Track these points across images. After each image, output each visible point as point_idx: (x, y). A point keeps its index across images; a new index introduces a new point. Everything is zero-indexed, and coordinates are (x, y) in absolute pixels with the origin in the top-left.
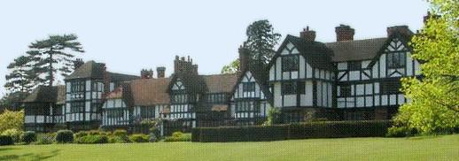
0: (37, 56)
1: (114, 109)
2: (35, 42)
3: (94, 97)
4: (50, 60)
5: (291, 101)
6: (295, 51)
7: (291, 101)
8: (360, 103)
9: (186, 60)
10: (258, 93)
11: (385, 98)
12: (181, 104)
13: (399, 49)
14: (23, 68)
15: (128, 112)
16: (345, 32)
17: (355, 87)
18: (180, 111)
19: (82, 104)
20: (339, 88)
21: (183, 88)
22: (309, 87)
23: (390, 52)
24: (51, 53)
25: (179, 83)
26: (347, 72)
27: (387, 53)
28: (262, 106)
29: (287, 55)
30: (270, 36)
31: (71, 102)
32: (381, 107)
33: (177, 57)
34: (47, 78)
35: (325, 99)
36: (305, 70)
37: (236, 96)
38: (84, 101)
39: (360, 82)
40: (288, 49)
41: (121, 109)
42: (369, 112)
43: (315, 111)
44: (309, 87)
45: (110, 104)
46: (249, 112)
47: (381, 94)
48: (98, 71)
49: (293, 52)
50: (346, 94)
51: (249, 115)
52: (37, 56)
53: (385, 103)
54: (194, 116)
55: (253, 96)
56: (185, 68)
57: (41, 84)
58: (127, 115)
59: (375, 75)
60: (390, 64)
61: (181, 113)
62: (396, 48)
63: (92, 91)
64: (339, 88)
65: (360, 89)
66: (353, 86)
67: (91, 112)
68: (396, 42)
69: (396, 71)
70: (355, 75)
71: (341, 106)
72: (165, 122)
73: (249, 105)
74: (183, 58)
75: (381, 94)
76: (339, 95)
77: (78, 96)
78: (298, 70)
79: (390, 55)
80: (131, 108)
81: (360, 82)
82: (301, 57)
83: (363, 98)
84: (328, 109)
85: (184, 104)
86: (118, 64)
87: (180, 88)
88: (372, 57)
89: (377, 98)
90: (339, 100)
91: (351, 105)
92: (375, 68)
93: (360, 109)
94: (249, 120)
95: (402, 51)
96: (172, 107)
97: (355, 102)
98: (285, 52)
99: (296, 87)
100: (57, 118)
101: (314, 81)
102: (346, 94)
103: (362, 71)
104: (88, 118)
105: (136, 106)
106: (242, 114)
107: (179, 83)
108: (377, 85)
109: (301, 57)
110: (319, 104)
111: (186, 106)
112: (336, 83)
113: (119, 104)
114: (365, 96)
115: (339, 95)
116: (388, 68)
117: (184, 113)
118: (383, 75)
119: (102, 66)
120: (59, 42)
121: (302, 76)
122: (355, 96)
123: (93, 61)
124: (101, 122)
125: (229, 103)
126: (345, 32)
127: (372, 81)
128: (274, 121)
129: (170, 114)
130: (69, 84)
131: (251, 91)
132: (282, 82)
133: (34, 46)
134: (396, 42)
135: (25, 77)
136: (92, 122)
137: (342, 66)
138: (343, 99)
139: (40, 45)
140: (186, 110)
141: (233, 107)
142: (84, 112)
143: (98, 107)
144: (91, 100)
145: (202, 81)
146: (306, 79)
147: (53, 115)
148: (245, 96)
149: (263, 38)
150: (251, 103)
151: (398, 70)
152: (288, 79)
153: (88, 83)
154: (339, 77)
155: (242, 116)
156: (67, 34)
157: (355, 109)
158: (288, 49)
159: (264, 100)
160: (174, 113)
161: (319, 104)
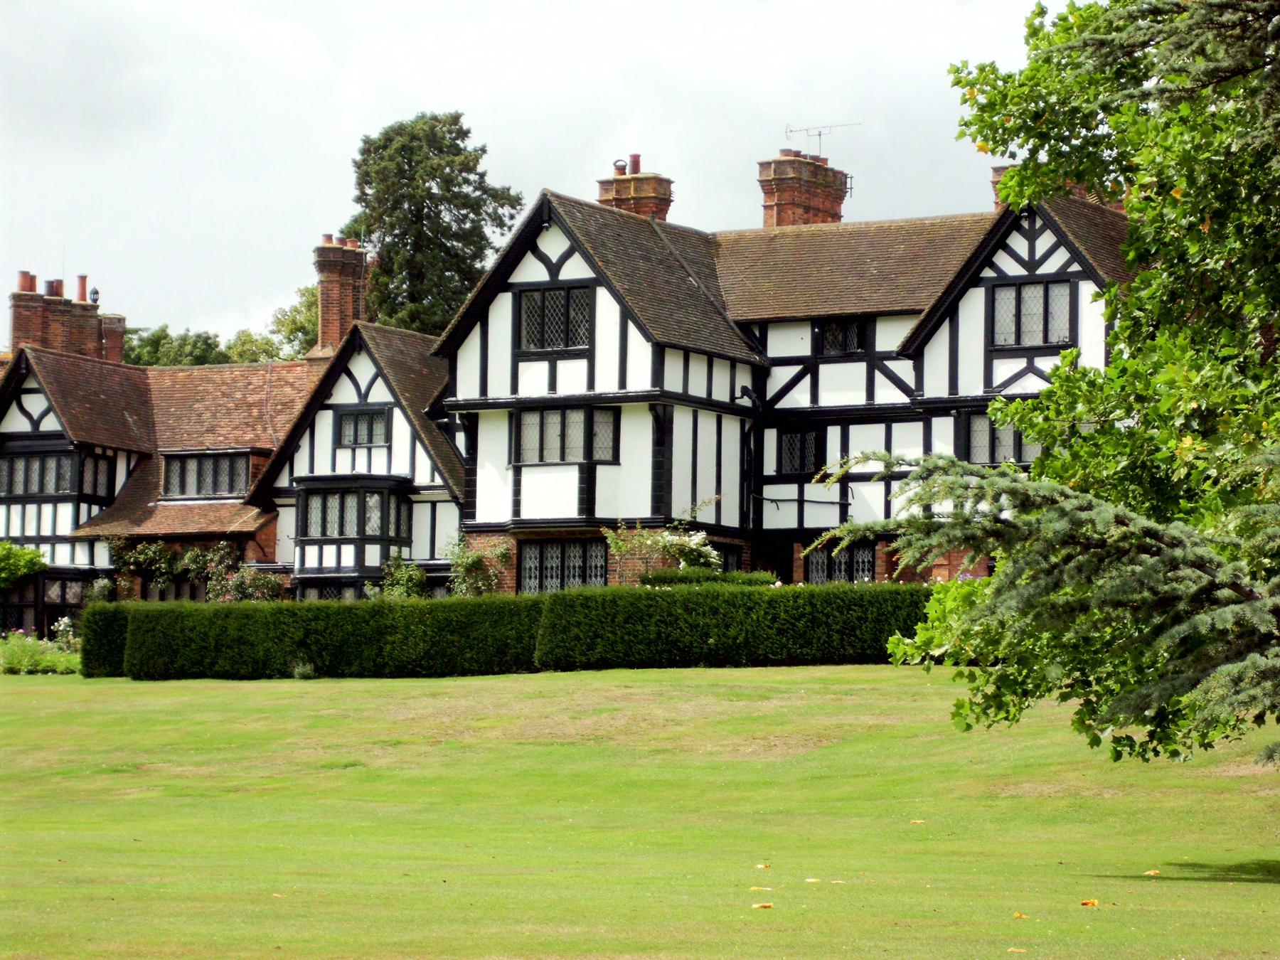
12: (40, 499)
16: (805, 186)
20: (771, 436)
21: (51, 424)
22: (637, 434)
23: (1004, 281)
26: (809, 367)
27: (992, 290)
28: (421, 514)
37: (301, 469)
39: (871, 414)
44: (637, 434)
46: (361, 542)
51: (360, 556)
54: (103, 560)
55: (379, 469)
64: (771, 436)
65: (866, 437)
66: (834, 433)
68: (1032, 237)
69: (1031, 369)
70: (842, 385)
71: (779, 517)
74: (55, 287)
76: (770, 468)
81: (871, 414)
85: (56, 500)
90: (770, 491)
92: (937, 352)
95: (1061, 277)
98: (531, 271)
101: (661, 406)
103: (876, 362)
106: (330, 550)
108: (944, 428)
109: (604, 298)
111: (66, 510)
112: (759, 414)
115: (770, 468)
116: (993, 351)
117: (55, 540)
121: (607, 384)
127: (922, 411)
134: (1032, 237)
137: (791, 343)
138: (791, 490)
140: (65, 528)
141: (287, 519)
148: (344, 469)
154: (773, 388)
155: (330, 561)
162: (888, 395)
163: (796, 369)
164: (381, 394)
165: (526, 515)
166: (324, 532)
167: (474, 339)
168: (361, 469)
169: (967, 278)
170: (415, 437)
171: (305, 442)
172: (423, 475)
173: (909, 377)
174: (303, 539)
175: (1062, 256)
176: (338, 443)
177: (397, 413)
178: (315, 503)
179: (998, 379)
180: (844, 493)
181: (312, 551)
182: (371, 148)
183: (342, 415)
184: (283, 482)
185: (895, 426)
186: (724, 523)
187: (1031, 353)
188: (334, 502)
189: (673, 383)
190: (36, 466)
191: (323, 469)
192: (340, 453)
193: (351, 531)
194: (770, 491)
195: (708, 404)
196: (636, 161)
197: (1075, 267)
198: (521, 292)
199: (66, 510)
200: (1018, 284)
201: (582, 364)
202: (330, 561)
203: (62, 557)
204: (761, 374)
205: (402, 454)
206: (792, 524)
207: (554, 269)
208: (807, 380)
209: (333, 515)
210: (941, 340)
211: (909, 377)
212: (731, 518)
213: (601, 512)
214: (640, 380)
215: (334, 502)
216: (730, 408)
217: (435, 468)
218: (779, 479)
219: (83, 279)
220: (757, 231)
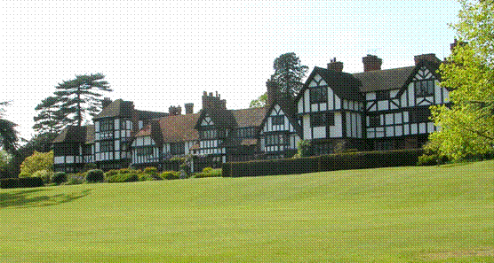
0: (65, 96)
2: (61, 83)
3: (123, 135)
4: (78, 100)
5: (320, 132)
6: (323, 83)
7: (320, 132)
8: (390, 133)
9: (214, 95)
10: (287, 126)
12: (210, 140)
16: (372, 62)
18: (209, 147)
19: (111, 143)
20: (368, 118)
21: (211, 123)
22: (338, 119)
24: (78, 93)
25: (208, 119)
26: (376, 102)
28: (292, 139)
31: (101, 141)
32: (410, 136)
34: (76, 118)
35: (355, 131)
36: (333, 101)
37: (265, 130)
38: (113, 140)
39: (389, 111)
44: (338, 119)
45: (139, 142)
46: (279, 145)
47: (410, 123)
50: (375, 124)
52: (65, 96)
53: (414, 131)
54: (224, 152)
55: (282, 129)
58: (156, 151)
59: (404, 105)
60: (419, 92)
63: (121, 129)
64: (368, 118)
65: (389, 119)
66: (382, 116)
67: (121, 151)
68: (424, 71)
69: (425, 100)
70: (383, 105)
72: (195, 158)
73: (279, 139)
74: (211, 94)
75: (410, 123)
77: (103, 136)
78: (326, 101)
79: (418, 83)
80: (160, 145)
81: (389, 111)
84: (357, 139)
89: (406, 126)
90: (368, 130)
91: (380, 135)
92: (404, 97)
93: (390, 139)
94: (278, 153)
96: (201, 143)
99: (325, 119)
100: (87, 158)
101: (343, 112)
103: (390, 100)
104: (117, 157)
107: (208, 119)
108: (406, 114)
109: (329, 88)
111: (216, 142)
112: (365, 113)
113: (148, 142)
114: (394, 125)
116: (416, 96)
118: (412, 104)
119: (130, 104)
121: (331, 108)
122: (384, 126)
125: (258, 137)
126: (372, 62)
127: (401, 110)
128: (304, 154)
129: (199, 150)
132: (311, 114)
133: (62, 86)
134: (424, 71)
135: (53, 117)
137: (371, 97)
139: (67, 85)
140: (216, 145)
141: (263, 141)
142: (114, 151)
143: (128, 145)
144: (120, 138)
147: (83, 156)
148: (274, 130)
149: (291, 70)
151: (427, 98)
153: (117, 122)
157: (385, 139)
159: (293, 133)
160: (204, 149)
161: (349, 135)
162: (393, 107)
164: (282, 113)
169: (410, 80)
184: (262, 133)
191: (270, 130)
198: (311, 89)
199: (216, 142)
204: (365, 103)
210: (404, 95)
214: (338, 107)
216: (358, 112)
218: (371, 127)
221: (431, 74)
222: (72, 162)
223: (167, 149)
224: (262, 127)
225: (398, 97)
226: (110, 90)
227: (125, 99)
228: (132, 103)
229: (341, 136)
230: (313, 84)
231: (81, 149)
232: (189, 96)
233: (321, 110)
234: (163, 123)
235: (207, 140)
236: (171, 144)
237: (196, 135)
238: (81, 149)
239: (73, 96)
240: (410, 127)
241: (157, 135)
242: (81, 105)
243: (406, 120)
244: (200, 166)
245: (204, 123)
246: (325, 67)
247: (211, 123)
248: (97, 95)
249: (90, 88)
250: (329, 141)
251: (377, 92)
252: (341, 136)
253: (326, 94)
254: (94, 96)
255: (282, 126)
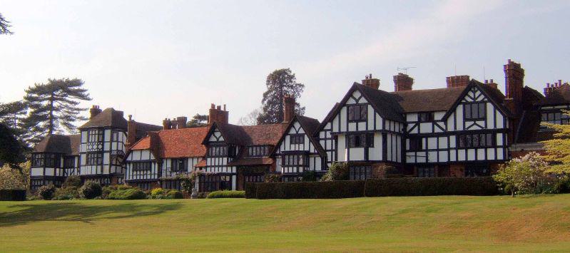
0: (36, 103)
1: (139, 162)
2: (33, 86)
3: (114, 148)
4: (50, 108)
5: (358, 154)
6: (363, 101)
7: (358, 154)
8: (433, 158)
9: (222, 109)
10: (307, 145)
11: (462, 153)
12: (219, 157)
13: (479, 99)
14: (17, 116)
15: (157, 165)
16: (403, 81)
17: (427, 141)
18: (219, 165)
19: (100, 156)
20: (408, 141)
21: (222, 139)
22: (378, 140)
23: (468, 103)
24: (52, 99)
25: (218, 134)
26: (418, 124)
27: (464, 104)
28: (312, 160)
29: (353, 105)
30: (292, 87)
31: (88, 153)
32: (457, 163)
33: (213, 106)
34: (46, 127)
35: (394, 155)
36: (374, 121)
37: (282, 149)
38: (102, 152)
39: (433, 135)
40: (355, 99)
41: (149, 162)
42: (443, 167)
43: (496, 177)
44: (378, 140)
45: (136, 156)
46: (298, 166)
47: (457, 148)
48: (116, 121)
49: (360, 102)
50: (417, 146)
51: (298, 170)
52: (36, 103)
53: (462, 158)
54: (234, 171)
55: (301, 149)
56: (218, 115)
57: (38, 134)
58: (155, 168)
59: (451, 128)
60: (468, 116)
61: (219, 166)
62: (474, 99)
63: (112, 141)
64: (408, 141)
65: (432, 143)
66: (424, 140)
67: (111, 165)
68: (474, 92)
69: (475, 124)
70: (426, 128)
71: (410, 160)
72: (201, 176)
73: (298, 160)
74: (219, 107)
75: (457, 148)
76: (408, 148)
77: (90, 147)
78: (366, 120)
79: (468, 107)
80: (160, 161)
81: (433, 135)
82: (370, 107)
83: (440, 152)
84: (396, 163)
85: (223, 157)
86: (148, 113)
87: (218, 139)
88: (447, 107)
89: (453, 153)
90: (407, 154)
91: (421, 160)
92: (336, 122)
93: (433, 164)
94: (298, 174)
95: (482, 101)
96: (209, 159)
97: (427, 157)
98: (351, 101)
99: (359, 140)
100: (69, 171)
101: (384, 133)
102: (417, 146)
103: (435, 123)
104: (106, 172)
105: (167, 159)
106: (291, 168)
107: (218, 134)
108: (453, 138)
109: (370, 107)
110: (389, 159)
111: (225, 159)
112: (405, 135)
113: (146, 156)
114: (438, 150)
115: (408, 148)
116: (465, 119)
117: (222, 166)
118: (460, 128)
119: (120, 114)
120: (68, 88)
121: (371, 128)
122: (427, 151)
123: (113, 109)
124: (122, 176)
125: (273, 156)
126: (403, 81)
127: (447, 134)
128: (335, 177)
129: (206, 167)
130: (85, 134)
131: (299, 143)
132: (348, 134)
133: (32, 91)
134: (474, 92)
135: (20, 125)
136: (111, 176)
137: (412, 118)
138: (413, 154)
139: (40, 90)
140: (225, 163)
141: (279, 162)
142: (102, 164)
143: (121, 159)
144: (111, 151)
145: (239, 130)
146: (375, 131)
147: (64, 168)
148: (293, 149)
149: (285, 88)
150: (301, 156)
151: (477, 122)
152: (355, 130)
153: (108, 133)
154: (408, 129)
155: (291, 171)
156: (71, 79)
157: (427, 165)
158: (355, 99)
159: (314, 154)
160: (211, 166)
161: (389, 159)
162: (437, 130)
163: (414, 124)
164: (302, 131)
165: (440, 161)
166: (298, 163)
167: (337, 118)
168: (297, 149)
169: (458, 102)
170: (310, 141)
171: (283, 143)
172: (312, 150)
173: (444, 127)
174: (283, 165)
175: (482, 97)
176: (291, 143)
177: (306, 135)
178: (287, 157)
179: (466, 127)
180: (427, 154)
181: (286, 169)
182: (269, 78)
183: (292, 136)
184: (278, 152)
185: (429, 139)
186: (459, 160)
187: (475, 120)
188: (291, 157)
189: (387, 128)
190: (218, 149)
191: (287, 149)
192: (292, 145)
193: (296, 164)
194: (407, 154)
195: (394, 132)
196: (371, 75)
197: (486, 100)
198: (348, 106)
199: (225, 159)
200: (471, 103)
201: (365, 123)
202: (295, 171)
203: (224, 170)
204: (406, 125)
205: (307, 145)
206: (414, 162)
207: (357, 101)
208: (417, 127)
209: (291, 160)
210: (452, 118)
211: (444, 127)
212: (399, 161)
213: (370, 159)
214: (379, 127)
215: (291, 157)
216: (398, 134)
217: (315, 148)
218: (411, 151)
219: (225, 105)
220: (439, 92)
221: (482, 97)
222: (52, 174)
223: (167, 165)
224: (279, 145)
225: (445, 120)
226: (89, 99)
227: (117, 109)
228: (355, 83)
229: (381, 159)
230: (351, 101)
231: (62, 160)
232: (194, 107)
233: (360, 129)
234: (165, 136)
235: (215, 157)
236: (173, 160)
237: (203, 150)
238: (62, 160)
239: (45, 103)
240: (111, 148)
241: (157, 148)
242: (54, 113)
243: (453, 144)
244: (212, 185)
245: (213, 139)
246: (361, 83)
247: (222, 139)
248: (72, 103)
249: (65, 95)
250: (367, 163)
251: (420, 113)
252: (381, 159)
253: (367, 113)
254: (69, 104)
255: (301, 145)
